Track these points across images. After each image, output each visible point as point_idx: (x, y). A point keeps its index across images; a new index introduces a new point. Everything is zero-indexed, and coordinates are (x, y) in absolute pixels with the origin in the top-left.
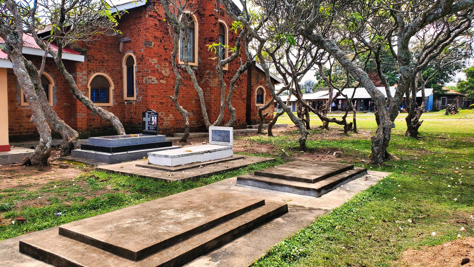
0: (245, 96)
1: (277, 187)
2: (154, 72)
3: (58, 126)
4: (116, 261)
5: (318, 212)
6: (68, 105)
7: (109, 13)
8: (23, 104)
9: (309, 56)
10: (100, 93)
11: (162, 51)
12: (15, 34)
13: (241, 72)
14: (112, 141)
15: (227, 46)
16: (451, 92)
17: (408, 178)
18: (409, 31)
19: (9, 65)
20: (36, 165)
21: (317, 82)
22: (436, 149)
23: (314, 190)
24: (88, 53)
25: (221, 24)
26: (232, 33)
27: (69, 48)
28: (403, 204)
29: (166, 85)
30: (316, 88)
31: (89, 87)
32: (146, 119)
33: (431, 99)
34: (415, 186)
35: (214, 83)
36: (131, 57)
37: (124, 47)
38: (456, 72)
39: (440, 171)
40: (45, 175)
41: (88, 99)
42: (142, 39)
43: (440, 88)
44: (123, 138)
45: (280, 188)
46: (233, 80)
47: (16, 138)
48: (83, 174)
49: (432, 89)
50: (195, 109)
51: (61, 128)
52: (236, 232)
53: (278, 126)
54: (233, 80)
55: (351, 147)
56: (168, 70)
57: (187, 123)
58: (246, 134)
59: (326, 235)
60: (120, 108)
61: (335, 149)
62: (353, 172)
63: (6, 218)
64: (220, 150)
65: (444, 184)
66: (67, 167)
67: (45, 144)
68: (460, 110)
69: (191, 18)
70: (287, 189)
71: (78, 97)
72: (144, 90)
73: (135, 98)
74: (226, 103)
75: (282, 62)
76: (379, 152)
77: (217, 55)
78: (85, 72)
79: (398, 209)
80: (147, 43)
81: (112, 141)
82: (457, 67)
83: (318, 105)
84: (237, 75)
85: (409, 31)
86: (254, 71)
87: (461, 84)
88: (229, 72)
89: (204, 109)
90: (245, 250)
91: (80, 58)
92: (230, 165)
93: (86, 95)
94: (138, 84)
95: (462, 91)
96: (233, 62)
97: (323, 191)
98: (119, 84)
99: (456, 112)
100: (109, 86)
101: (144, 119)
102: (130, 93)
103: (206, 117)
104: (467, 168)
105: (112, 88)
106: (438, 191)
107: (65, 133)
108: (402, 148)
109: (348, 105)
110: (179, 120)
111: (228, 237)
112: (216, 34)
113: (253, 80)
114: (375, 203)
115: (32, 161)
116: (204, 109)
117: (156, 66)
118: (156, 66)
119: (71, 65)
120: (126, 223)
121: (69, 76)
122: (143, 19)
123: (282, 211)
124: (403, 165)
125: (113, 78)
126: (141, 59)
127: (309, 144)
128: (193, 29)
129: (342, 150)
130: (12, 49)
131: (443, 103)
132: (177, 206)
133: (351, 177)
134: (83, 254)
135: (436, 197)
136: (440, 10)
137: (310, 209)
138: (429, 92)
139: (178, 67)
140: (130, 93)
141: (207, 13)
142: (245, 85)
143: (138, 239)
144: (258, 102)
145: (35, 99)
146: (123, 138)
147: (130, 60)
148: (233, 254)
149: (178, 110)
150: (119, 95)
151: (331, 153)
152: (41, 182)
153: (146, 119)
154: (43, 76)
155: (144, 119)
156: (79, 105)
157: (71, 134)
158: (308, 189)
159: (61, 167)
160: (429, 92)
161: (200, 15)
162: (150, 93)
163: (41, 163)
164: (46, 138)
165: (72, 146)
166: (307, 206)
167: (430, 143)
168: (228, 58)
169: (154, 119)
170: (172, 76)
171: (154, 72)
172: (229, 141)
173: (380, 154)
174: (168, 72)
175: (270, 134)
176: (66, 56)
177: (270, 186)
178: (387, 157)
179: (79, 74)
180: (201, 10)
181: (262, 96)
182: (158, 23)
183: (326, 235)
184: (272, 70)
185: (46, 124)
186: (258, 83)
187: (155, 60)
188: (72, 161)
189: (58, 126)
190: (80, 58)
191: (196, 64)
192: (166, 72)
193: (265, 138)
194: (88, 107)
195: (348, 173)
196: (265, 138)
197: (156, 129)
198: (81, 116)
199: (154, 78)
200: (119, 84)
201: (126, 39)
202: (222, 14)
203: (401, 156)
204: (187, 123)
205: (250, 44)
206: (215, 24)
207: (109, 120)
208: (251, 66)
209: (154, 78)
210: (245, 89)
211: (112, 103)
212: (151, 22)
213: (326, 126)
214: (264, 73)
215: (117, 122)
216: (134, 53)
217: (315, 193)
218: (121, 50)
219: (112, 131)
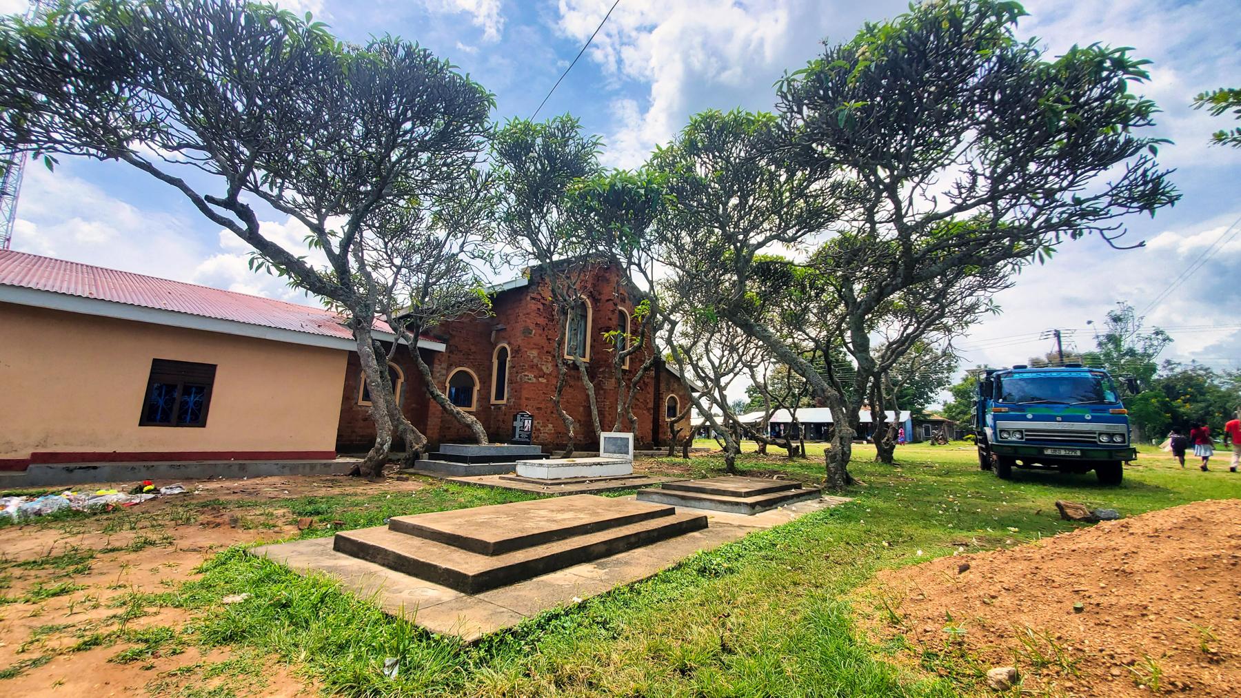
0: (651, 405)
1: (693, 503)
2: (533, 367)
3: (401, 427)
4: (463, 556)
5: (748, 530)
6: (418, 405)
7: (484, 292)
8: (361, 403)
9: (735, 355)
10: (462, 395)
11: (543, 342)
12: (367, 306)
13: (646, 369)
14: (471, 450)
15: (628, 335)
16: (936, 417)
17: (880, 504)
18: (863, 307)
19: (353, 347)
20: (366, 475)
21: (749, 401)
22: (920, 477)
23: (746, 504)
24: (451, 342)
25: (621, 312)
26: (634, 320)
27: (427, 335)
28: (874, 528)
29: (546, 386)
30: (747, 409)
31: (448, 385)
32: (517, 424)
33: (909, 426)
34: (892, 512)
35: (610, 384)
36: (504, 348)
37: (497, 337)
38: (939, 389)
39: (928, 499)
40: (376, 486)
41: (445, 396)
42: (520, 327)
43: (919, 411)
44: (485, 447)
45: (697, 504)
46: (635, 379)
47: (343, 447)
48: (428, 487)
49: (908, 412)
50: (583, 419)
51: (405, 431)
52: (633, 540)
53: (697, 450)
54: (635, 379)
55: (798, 470)
56: (550, 365)
57: (572, 434)
58: (652, 456)
59: (763, 553)
60: (485, 414)
61: (776, 472)
62: (799, 491)
63: (321, 521)
64: (614, 463)
65: (932, 510)
66: (407, 479)
67: (382, 445)
68: (950, 439)
69: (584, 304)
70: (708, 504)
71: (432, 393)
72: (516, 392)
73: (504, 402)
74: (625, 410)
75: (700, 364)
76: (837, 469)
77: (615, 346)
78: (444, 365)
79: (868, 532)
80: (527, 331)
81: (471, 450)
82: (940, 383)
83: (750, 432)
84: (640, 372)
85: (863, 307)
86: (663, 375)
87: (948, 409)
88: (630, 371)
89: (595, 412)
90: (644, 560)
91: (441, 347)
92: (629, 483)
93: (444, 392)
94: (511, 382)
95: (953, 418)
96: (636, 354)
97: (758, 508)
98: (486, 382)
99: (946, 441)
100: (474, 385)
101: (515, 424)
102: (500, 395)
103: (597, 424)
104: (966, 497)
105: (477, 388)
106: (925, 517)
107: (410, 437)
108: (872, 474)
109: (792, 433)
110: (561, 433)
111: (621, 545)
112: (614, 322)
113: (663, 386)
114: (834, 526)
115: (362, 469)
116: (595, 412)
117: (535, 361)
118: (535, 361)
119: (429, 355)
120: (480, 519)
121: (424, 366)
122: (524, 302)
123: (699, 524)
124: (872, 490)
125: (479, 375)
126: (516, 352)
127: (738, 464)
128: (585, 317)
129: (785, 473)
130: (360, 323)
131: (927, 430)
132: (554, 508)
133: (798, 497)
134: (419, 548)
135: (921, 522)
136: (899, 280)
137: (739, 526)
138: (905, 416)
139: (565, 363)
140: (500, 395)
141: (604, 297)
142: (651, 390)
143: (494, 531)
144: (669, 416)
145: (378, 386)
146: (485, 447)
147: (503, 354)
148: (626, 563)
149: (561, 415)
150: (485, 397)
151: (771, 476)
152: (370, 492)
153: (517, 424)
154: (391, 368)
155: (515, 424)
156: (434, 407)
157: (418, 440)
158: (737, 504)
159: (398, 479)
160: (905, 416)
161: (595, 300)
162: (525, 394)
163: (375, 473)
164: (384, 439)
165: (417, 456)
166: (736, 523)
167: (910, 470)
168: (629, 349)
169: (528, 423)
170: (554, 374)
171: (533, 367)
172: (627, 453)
173: (840, 476)
174: (551, 369)
175: (686, 456)
176: (423, 344)
177: (683, 502)
178: (849, 481)
179: (437, 367)
180: (595, 293)
181: (674, 408)
182: (541, 307)
183: (763, 553)
184: (689, 374)
185: (387, 418)
186: (669, 390)
187: (535, 353)
188: (414, 474)
189: (401, 427)
190: (441, 347)
191: (587, 359)
192: (548, 368)
193: (681, 460)
194: (444, 407)
195: (793, 491)
196: (681, 460)
197: (529, 437)
198: (433, 422)
199: (531, 376)
200: (486, 382)
201: (500, 327)
202: (623, 300)
203: (870, 483)
204: (572, 434)
205: (658, 334)
206: (613, 311)
207: (469, 426)
208: (658, 364)
209: (531, 376)
210: (651, 396)
211: (473, 408)
212: (533, 306)
213: (763, 450)
214: (680, 380)
215: (479, 428)
216: (509, 344)
217: (748, 509)
218: (492, 339)
219: (474, 440)
